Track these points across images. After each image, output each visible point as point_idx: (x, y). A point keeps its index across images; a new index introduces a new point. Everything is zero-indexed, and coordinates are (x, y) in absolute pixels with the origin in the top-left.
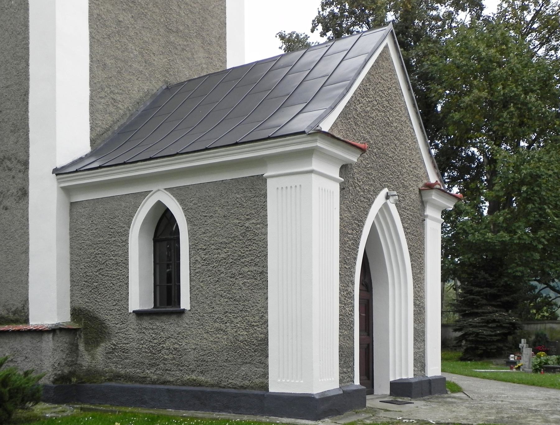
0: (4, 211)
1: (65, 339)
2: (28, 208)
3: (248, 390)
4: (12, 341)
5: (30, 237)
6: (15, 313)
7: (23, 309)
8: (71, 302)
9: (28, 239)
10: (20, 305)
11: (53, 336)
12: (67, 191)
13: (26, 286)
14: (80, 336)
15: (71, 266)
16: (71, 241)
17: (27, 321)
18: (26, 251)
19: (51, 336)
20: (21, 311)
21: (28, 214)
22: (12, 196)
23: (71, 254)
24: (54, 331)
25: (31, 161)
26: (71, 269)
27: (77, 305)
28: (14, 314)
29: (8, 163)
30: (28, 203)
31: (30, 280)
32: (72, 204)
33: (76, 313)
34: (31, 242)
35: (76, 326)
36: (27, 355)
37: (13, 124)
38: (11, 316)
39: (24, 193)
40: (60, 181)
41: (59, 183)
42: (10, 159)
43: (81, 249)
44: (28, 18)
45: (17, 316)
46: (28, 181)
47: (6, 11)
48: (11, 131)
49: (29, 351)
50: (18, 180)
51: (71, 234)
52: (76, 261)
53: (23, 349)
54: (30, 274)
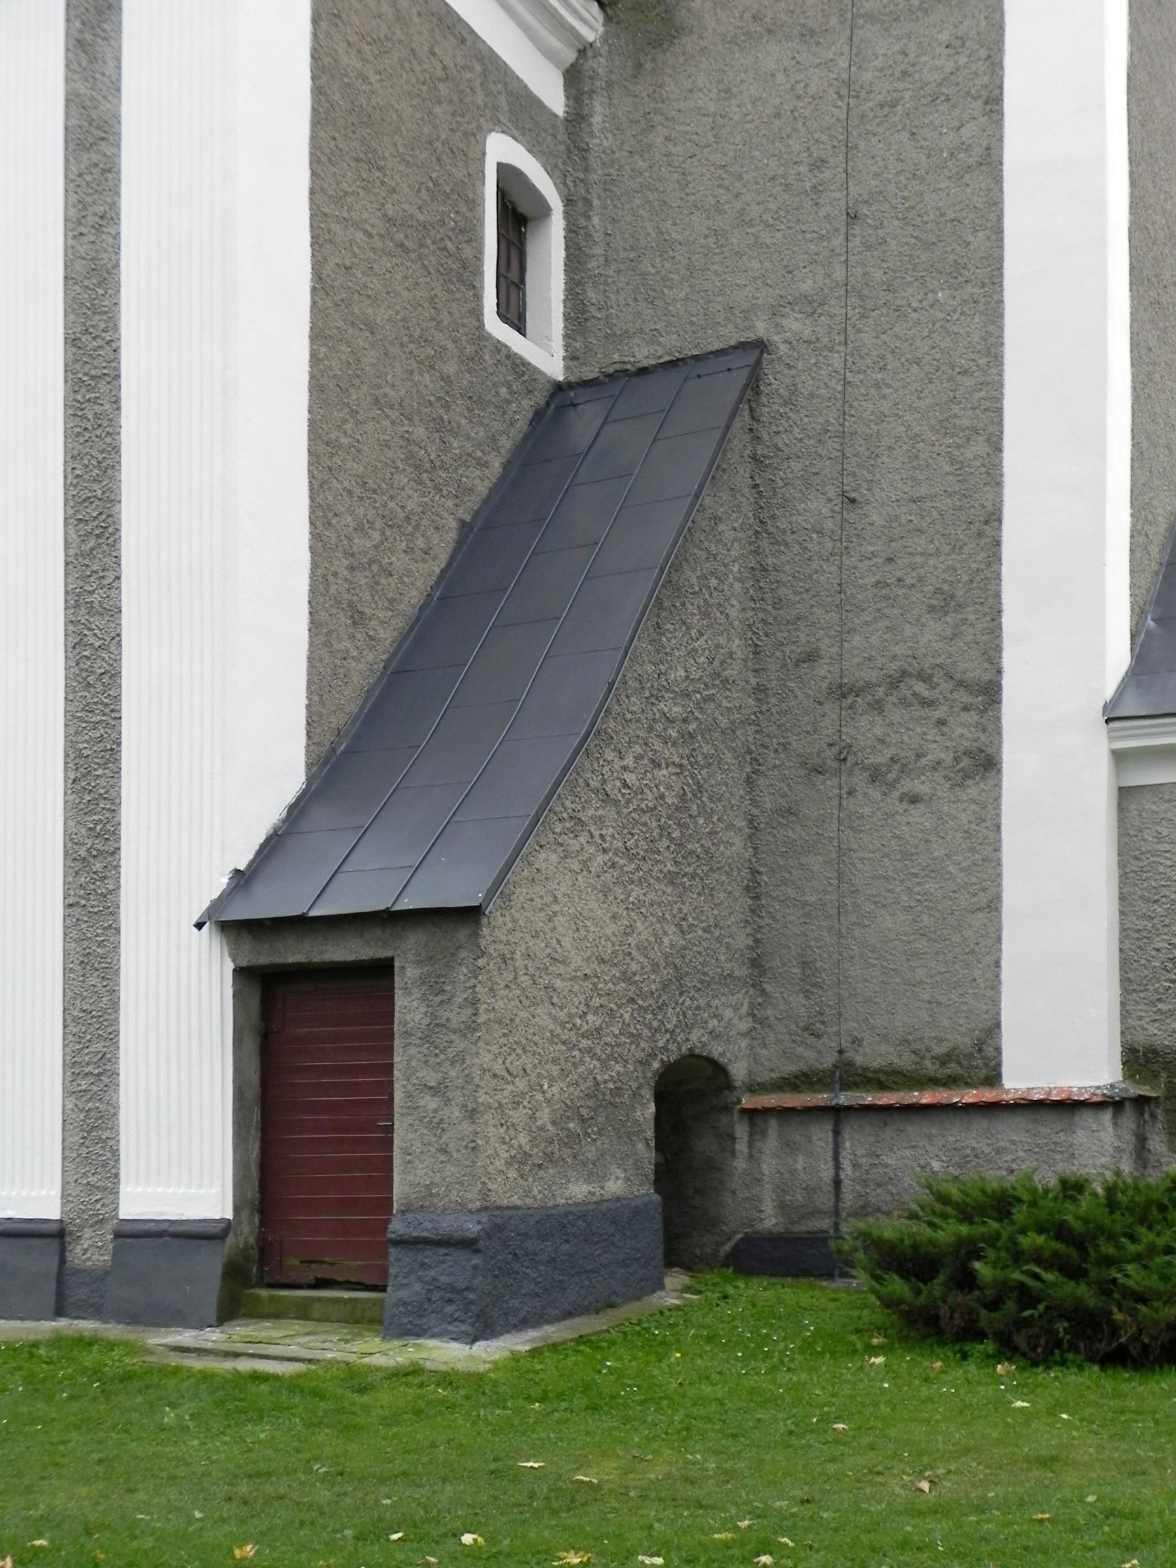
0: (905, 805)
1: (1128, 1120)
2: (998, 799)
3: (569, 1335)
4: (955, 1132)
5: (1006, 870)
6: (943, 1060)
7: (980, 1050)
8: (1122, 1033)
9: (1000, 875)
10: (967, 1040)
11: (1115, 1116)
12: (1119, 758)
13: (991, 993)
14: (1153, 1116)
15: (1121, 942)
16: (1120, 882)
17: (993, 1078)
18: (994, 905)
19: (1107, 1116)
20: (970, 1056)
21: (998, 815)
22: (935, 769)
23: (1122, 913)
24: (1111, 1104)
25: (1006, 682)
26: (1121, 950)
27: (1140, 1038)
28: (943, 1064)
29: (920, 687)
30: (998, 786)
31: (1004, 976)
32: (1121, 789)
33: (1137, 1059)
34: (1006, 883)
35: (1135, 1090)
36: (1014, 1166)
37: (938, 591)
38: (930, 1067)
39: (986, 763)
40: (1115, 734)
41: (1111, 739)
42: (924, 677)
43: (1156, 901)
44: (1000, 337)
45: (953, 1068)
46: (1000, 734)
47: (915, 315)
48: (932, 609)
49: (1021, 1154)
50: (959, 731)
51: (1122, 865)
52: (1138, 931)
53: (998, 1151)
54: (1003, 964)
